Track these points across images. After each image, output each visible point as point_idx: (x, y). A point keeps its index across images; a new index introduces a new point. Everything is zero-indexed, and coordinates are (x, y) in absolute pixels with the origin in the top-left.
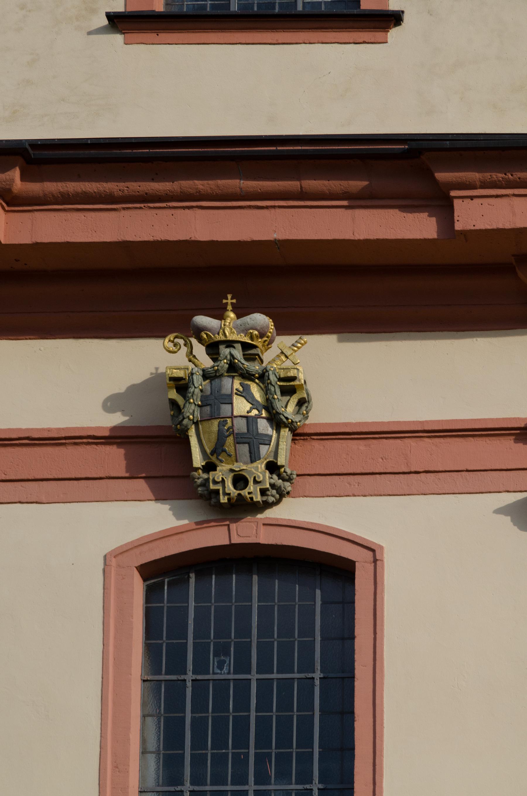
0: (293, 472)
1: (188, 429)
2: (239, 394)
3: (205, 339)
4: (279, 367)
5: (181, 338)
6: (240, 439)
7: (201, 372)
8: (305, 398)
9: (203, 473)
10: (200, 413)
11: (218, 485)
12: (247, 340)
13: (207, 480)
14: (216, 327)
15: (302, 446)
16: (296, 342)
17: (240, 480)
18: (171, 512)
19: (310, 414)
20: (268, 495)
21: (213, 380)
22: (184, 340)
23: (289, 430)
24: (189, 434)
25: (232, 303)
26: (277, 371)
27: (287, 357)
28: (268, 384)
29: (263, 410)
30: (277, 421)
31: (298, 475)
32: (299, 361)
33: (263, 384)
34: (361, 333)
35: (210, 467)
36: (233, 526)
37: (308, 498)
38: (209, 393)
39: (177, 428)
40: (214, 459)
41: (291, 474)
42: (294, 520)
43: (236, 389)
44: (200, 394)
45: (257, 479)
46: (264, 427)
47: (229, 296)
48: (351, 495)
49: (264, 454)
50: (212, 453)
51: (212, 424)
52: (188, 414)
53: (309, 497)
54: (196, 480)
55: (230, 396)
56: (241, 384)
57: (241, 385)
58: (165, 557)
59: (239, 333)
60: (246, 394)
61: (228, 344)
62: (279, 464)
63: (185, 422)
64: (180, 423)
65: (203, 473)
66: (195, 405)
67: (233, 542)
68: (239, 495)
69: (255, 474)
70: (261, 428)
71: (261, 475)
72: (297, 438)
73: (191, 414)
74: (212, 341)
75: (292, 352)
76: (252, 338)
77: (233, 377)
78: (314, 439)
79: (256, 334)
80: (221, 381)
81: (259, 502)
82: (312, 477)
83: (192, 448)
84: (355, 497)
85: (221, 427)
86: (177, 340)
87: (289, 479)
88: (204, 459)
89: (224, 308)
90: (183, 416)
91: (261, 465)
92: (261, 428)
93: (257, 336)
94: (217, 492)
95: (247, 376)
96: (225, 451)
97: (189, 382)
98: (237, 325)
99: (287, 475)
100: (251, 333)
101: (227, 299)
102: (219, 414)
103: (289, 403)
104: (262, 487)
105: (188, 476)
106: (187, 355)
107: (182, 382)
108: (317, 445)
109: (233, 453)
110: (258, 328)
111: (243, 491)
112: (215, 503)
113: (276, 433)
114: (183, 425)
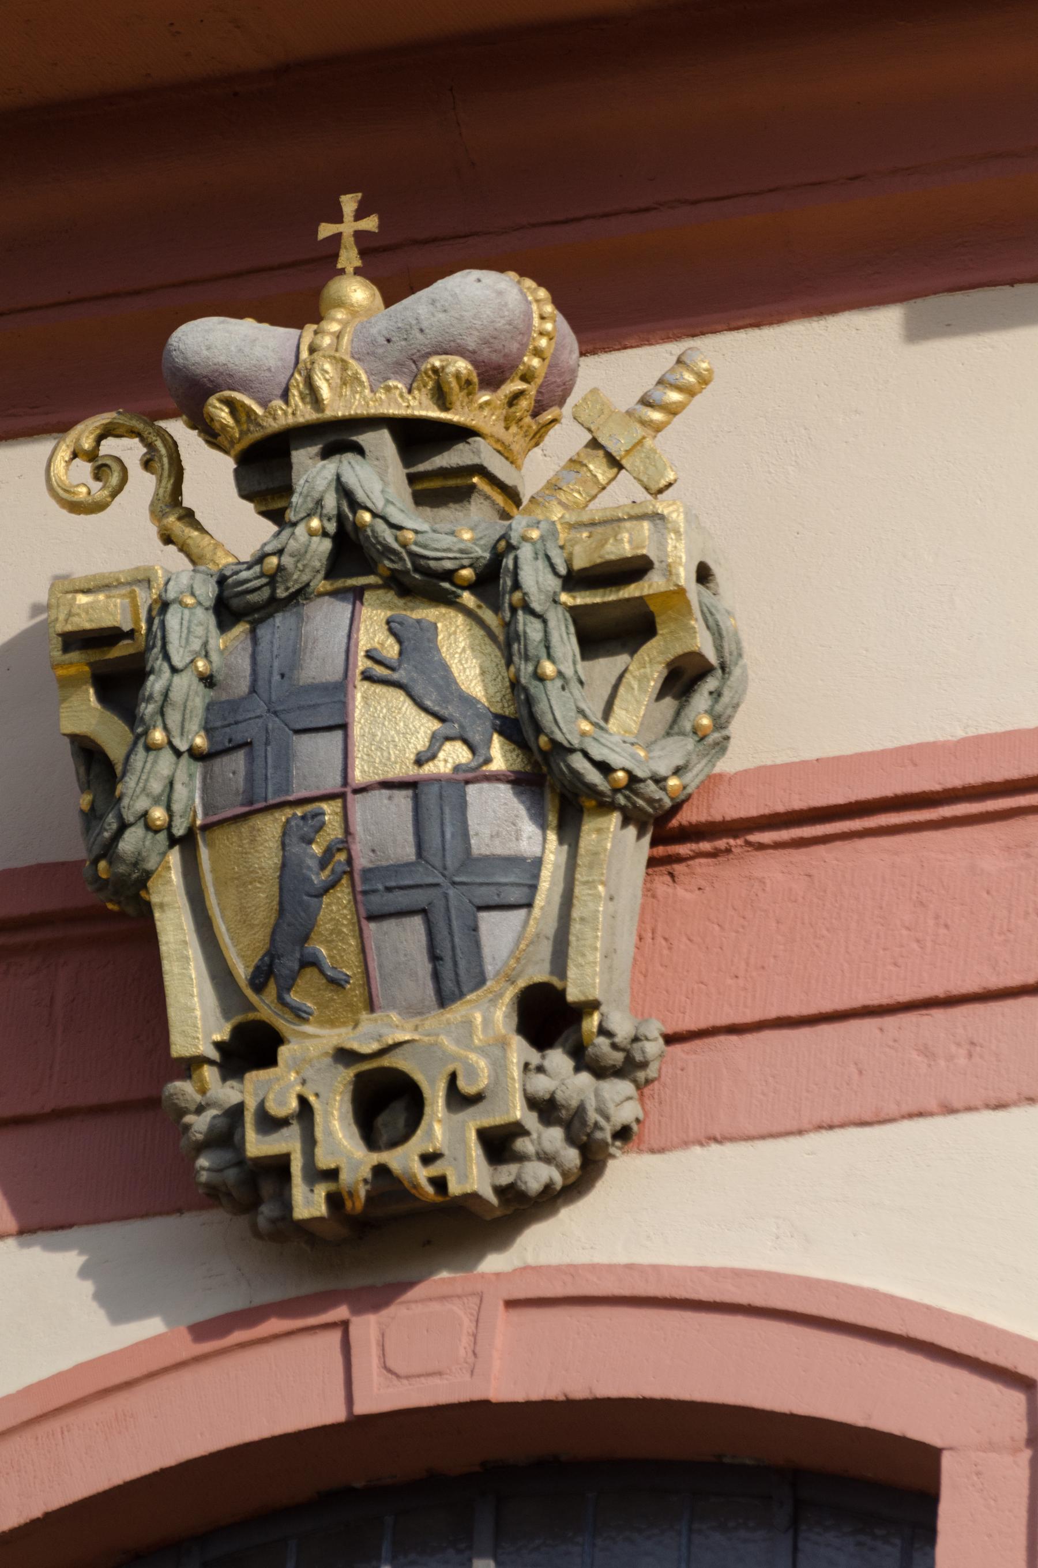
0: (643, 1031)
1: (148, 875)
2: (382, 675)
3: (224, 427)
4: (572, 517)
5: (133, 433)
6: (383, 898)
7: (208, 591)
8: (697, 656)
9: (224, 1078)
10: (205, 789)
11: (285, 1131)
12: (421, 407)
13: (237, 1112)
14: (272, 362)
15: (706, 884)
16: (660, 382)
17: (386, 1099)
18: (88, 1287)
19: (734, 729)
20: (520, 1158)
21: (261, 621)
22: (143, 440)
23: (626, 822)
24: (155, 899)
25: (358, 235)
26: (563, 536)
27: (615, 463)
28: (514, 610)
29: (496, 739)
30: (558, 787)
31: (670, 1039)
32: (671, 476)
33: (496, 609)
34: (1012, 284)
35: (251, 1048)
36: (367, 1327)
37: (728, 1150)
38: (242, 687)
39: (97, 878)
40: (265, 1008)
41: (636, 1039)
42: (655, 1268)
43: (369, 655)
44: (199, 699)
45: (462, 1084)
46: (501, 822)
47: (349, 203)
48: (933, 1105)
49: (504, 953)
50: (260, 979)
51: (253, 841)
52: (141, 804)
53: (732, 1139)
54: (189, 1119)
55: (337, 693)
56: (393, 628)
57: (392, 632)
58: (47, 1515)
59: (379, 379)
60: (408, 669)
61: (332, 438)
62: (573, 995)
63: (131, 842)
64: (108, 850)
65: (224, 1078)
66: (178, 754)
67: (361, 1408)
68: (381, 1171)
69: (455, 1058)
70: (486, 831)
71: (482, 1063)
72: (683, 849)
73: (156, 801)
74: (257, 435)
75: (639, 431)
76: (441, 397)
77: (357, 595)
78: (761, 847)
79: (458, 376)
80: (300, 619)
81: (475, 1196)
82: (749, 1038)
83: (166, 965)
84: (951, 1120)
85: (296, 848)
86: (110, 446)
87: (629, 1067)
88: (227, 1013)
89: (325, 262)
90: (120, 817)
91: (489, 1017)
92: (486, 831)
93: (466, 384)
94: (278, 1168)
95: (423, 582)
96: (311, 962)
97: (149, 648)
98: (373, 342)
99: (615, 1046)
100: (435, 371)
101: (337, 217)
102: (286, 785)
103: (622, 690)
104: (488, 1121)
105: (154, 1103)
106: (152, 512)
107: (122, 649)
108: (773, 873)
109: (351, 969)
110: (471, 343)
111: (400, 1151)
112: (273, 1221)
113: (561, 842)
114: (121, 859)
